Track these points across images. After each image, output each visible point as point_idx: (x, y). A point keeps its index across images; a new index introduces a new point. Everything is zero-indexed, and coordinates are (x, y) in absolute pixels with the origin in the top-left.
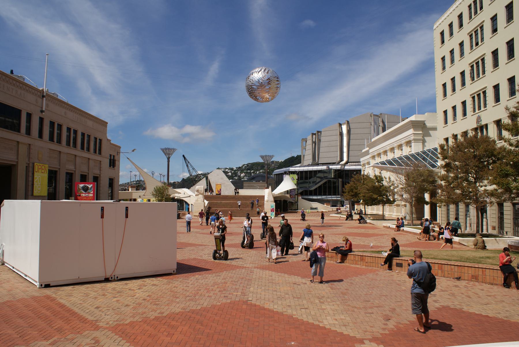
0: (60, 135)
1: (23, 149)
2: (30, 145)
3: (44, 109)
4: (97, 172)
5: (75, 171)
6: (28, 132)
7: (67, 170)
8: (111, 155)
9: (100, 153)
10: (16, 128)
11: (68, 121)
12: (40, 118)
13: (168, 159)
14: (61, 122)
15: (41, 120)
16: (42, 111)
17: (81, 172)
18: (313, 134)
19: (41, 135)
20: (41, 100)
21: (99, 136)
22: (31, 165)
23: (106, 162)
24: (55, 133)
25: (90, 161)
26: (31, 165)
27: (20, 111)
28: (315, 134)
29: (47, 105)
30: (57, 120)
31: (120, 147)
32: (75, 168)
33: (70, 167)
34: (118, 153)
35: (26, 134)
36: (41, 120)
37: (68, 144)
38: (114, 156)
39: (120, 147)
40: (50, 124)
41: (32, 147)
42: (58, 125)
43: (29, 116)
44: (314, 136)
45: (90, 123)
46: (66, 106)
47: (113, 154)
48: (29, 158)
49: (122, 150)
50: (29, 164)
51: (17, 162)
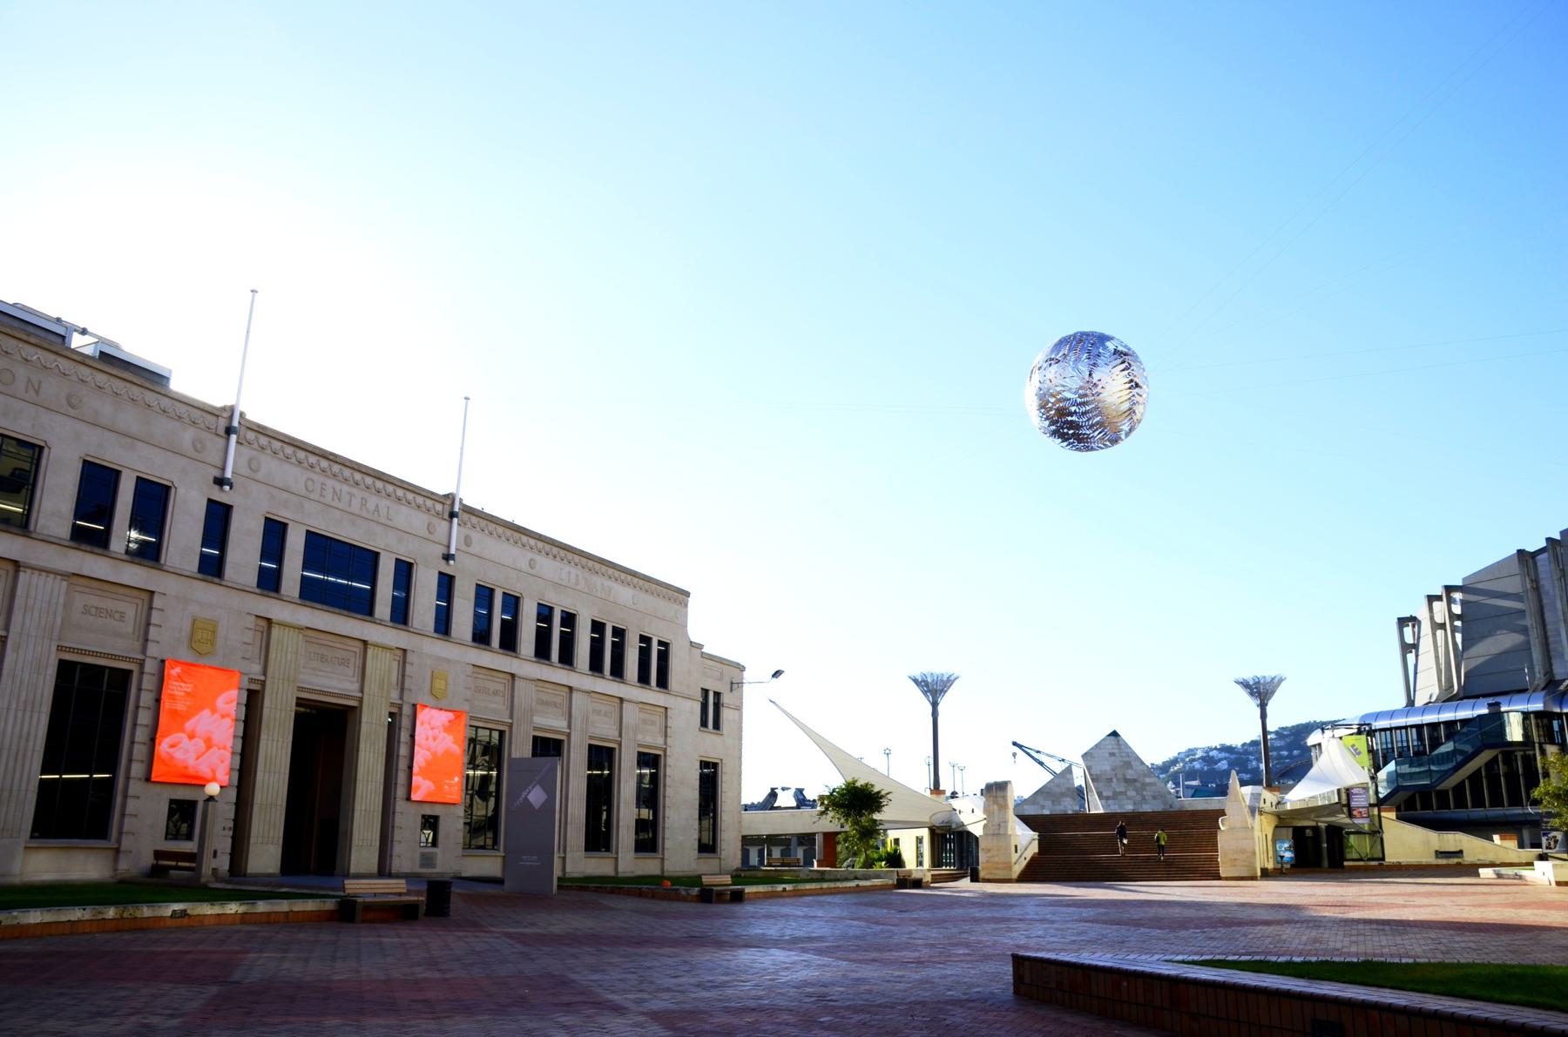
0: (568, 643)
1: (381, 666)
2: (405, 651)
3: (453, 551)
4: (651, 740)
5: (569, 735)
6: (401, 614)
7: (535, 729)
8: (705, 692)
9: (663, 682)
10: (363, 606)
11: (539, 586)
12: (269, 522)
13: (935, 705)
14: (515, 589)
15: (446, 584)
16: (447, 557)
17: (591, 738)
18: (1431, 599)
19: (443, 624)
20: (445, 524)
21: (657, 633)
22: (407, 710)
23: (686, 712)
24: (497, 622)
25: (575, 695)
26: (407, 710)
27: (375, 556)
28: (1439, 598)
29: (467, 541)
30: (502, 583)
31: (742, 669)
32: (569, 727)
33: (605, 731)
34: (736, 685)
35: (436, 631)
36: (446, 584)
37: (644, 678)
38: (717, 695)
39: (742, 669)
40: (477, 595)
41: (410, 657)
42: (660, 643)
43: (404, 572)
44: (1436, 604)
45: (624, 594)
46: (532, 542)
47: (713, 686)
48: (402, 689)
49: (747, 676)
50: (400, 707)
51: (361, 700)
